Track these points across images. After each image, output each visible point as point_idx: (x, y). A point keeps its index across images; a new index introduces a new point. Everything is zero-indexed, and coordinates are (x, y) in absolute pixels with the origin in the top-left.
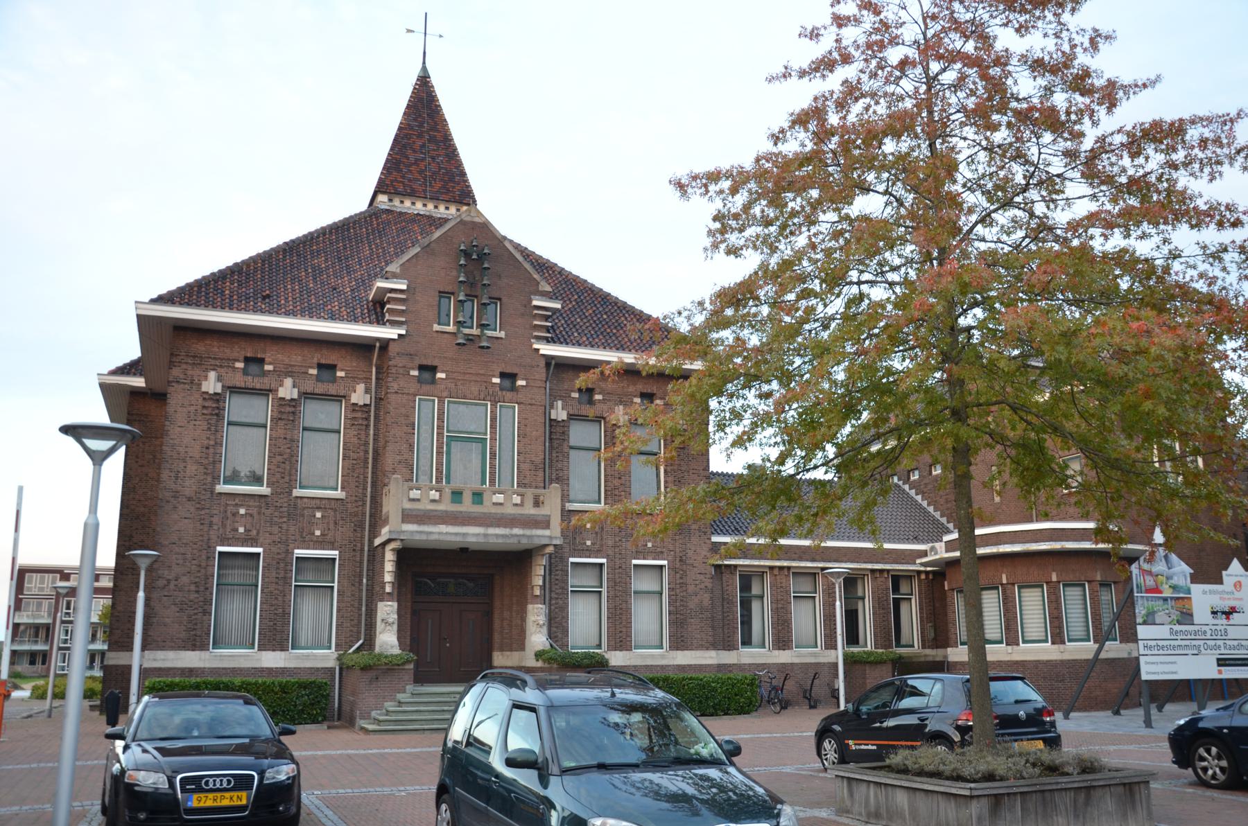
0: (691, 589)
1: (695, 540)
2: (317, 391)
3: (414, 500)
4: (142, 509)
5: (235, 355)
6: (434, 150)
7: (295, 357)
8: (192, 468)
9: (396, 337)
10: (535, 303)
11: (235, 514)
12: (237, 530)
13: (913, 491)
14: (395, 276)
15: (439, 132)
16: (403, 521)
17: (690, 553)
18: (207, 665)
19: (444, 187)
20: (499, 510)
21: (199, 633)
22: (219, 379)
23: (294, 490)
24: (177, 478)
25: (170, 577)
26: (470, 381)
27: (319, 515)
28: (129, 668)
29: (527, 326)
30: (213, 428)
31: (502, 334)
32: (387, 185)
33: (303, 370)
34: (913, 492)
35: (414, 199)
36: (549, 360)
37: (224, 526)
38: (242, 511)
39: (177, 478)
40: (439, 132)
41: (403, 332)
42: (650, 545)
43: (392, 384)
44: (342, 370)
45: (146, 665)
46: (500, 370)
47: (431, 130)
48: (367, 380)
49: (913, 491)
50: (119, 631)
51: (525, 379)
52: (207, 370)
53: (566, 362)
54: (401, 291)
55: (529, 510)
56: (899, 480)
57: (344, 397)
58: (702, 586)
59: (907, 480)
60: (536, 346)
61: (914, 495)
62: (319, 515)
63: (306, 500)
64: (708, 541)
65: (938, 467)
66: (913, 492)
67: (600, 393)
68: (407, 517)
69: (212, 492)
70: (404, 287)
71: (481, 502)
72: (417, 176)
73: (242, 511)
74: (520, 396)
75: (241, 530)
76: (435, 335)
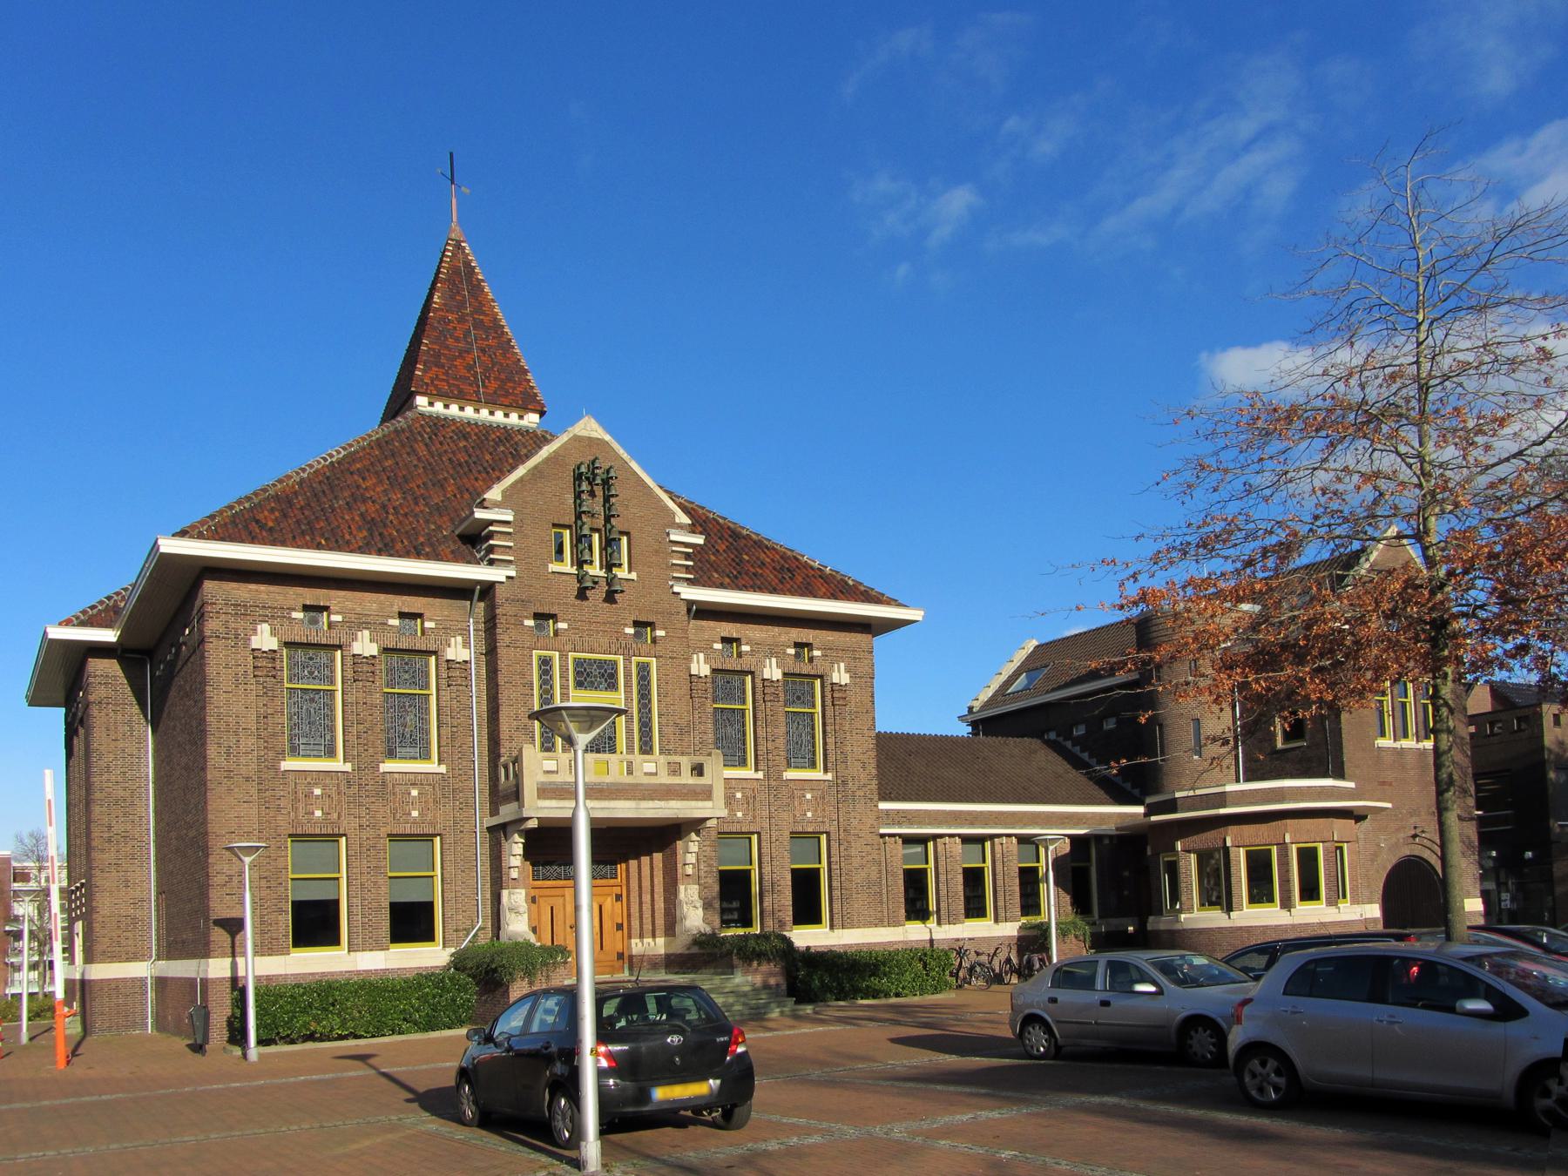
0: (856, 862)
1: (860, 807)
2: (400, 646)
3: (548, 772)
4: (121, 793)
5: (291, 603)
6: (482, 339)
7: (371, 602)
8: (249, 743)
9: (504, 579)
10: (673, 537)
11: (309, 795)
12: (313, 813)
13: (1078, 748)
14: (497, 505)
15: (487, 315)
16: (539, 798)
17: (855, 822)
18: (290, 971)
19: (500, 387)
20: (654, 780)
21: (274, 936)
22: (273, 633)
23: (381, 765)
24: (228, 754)
25: (232, 873)
26: (598, 632)
27: (415, 793)
28: (161, 983)
29: (664, 566)
30: (270, 694)
31: (634, 576)
32: (427, 384)
33: (381, 620)
34: (1077, 749)
35: (492, 407)
36: (690, 603)
37: (295, 809)
38: (318, 792)
39: (228, 754)
40: (487, 315)
41: (513, 574)
42: (809, 814)
43: (502, 637)
44: (431, 620)
45: (30, 991)
46: (633, 618)
47: (476, 313)
48: (465, 632)
49: (1078, 748)
50: (106, 940)
51: (664, 629)
52: (254, 623)
53: (243, 568)
54: (506, 523)
55: (687, 779)
56: (1058, 735)
57: (435, 653)
58: (870, 858)
59: (1069, 736)
60: (676, 589)
61: (1078, 753)
62: (415, 793)
63: (396, 776)
64: (875, 809)
65: (1114, 720)
66: (1077, 749)
67: (747, 644)
68: (545, 792)
69: (277, 769)
70: (510, 518)
71: (701, 774)
72: (463, 372)
73: (318, 792)
74: (658, 648)
75: (318, 813)
76: (550, 576)
